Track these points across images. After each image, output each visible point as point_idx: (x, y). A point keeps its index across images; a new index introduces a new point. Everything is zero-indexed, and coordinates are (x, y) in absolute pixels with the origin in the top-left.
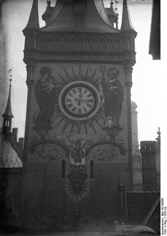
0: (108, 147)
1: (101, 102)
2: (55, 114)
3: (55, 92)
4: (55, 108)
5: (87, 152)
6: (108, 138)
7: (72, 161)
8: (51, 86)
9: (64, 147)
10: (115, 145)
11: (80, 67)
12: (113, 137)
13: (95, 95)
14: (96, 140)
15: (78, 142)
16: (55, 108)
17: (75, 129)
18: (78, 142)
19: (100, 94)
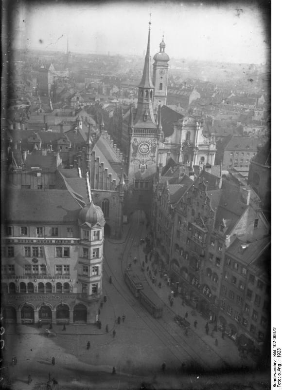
7: (141, 165)
8: (137, 144)
19: (150, 147)
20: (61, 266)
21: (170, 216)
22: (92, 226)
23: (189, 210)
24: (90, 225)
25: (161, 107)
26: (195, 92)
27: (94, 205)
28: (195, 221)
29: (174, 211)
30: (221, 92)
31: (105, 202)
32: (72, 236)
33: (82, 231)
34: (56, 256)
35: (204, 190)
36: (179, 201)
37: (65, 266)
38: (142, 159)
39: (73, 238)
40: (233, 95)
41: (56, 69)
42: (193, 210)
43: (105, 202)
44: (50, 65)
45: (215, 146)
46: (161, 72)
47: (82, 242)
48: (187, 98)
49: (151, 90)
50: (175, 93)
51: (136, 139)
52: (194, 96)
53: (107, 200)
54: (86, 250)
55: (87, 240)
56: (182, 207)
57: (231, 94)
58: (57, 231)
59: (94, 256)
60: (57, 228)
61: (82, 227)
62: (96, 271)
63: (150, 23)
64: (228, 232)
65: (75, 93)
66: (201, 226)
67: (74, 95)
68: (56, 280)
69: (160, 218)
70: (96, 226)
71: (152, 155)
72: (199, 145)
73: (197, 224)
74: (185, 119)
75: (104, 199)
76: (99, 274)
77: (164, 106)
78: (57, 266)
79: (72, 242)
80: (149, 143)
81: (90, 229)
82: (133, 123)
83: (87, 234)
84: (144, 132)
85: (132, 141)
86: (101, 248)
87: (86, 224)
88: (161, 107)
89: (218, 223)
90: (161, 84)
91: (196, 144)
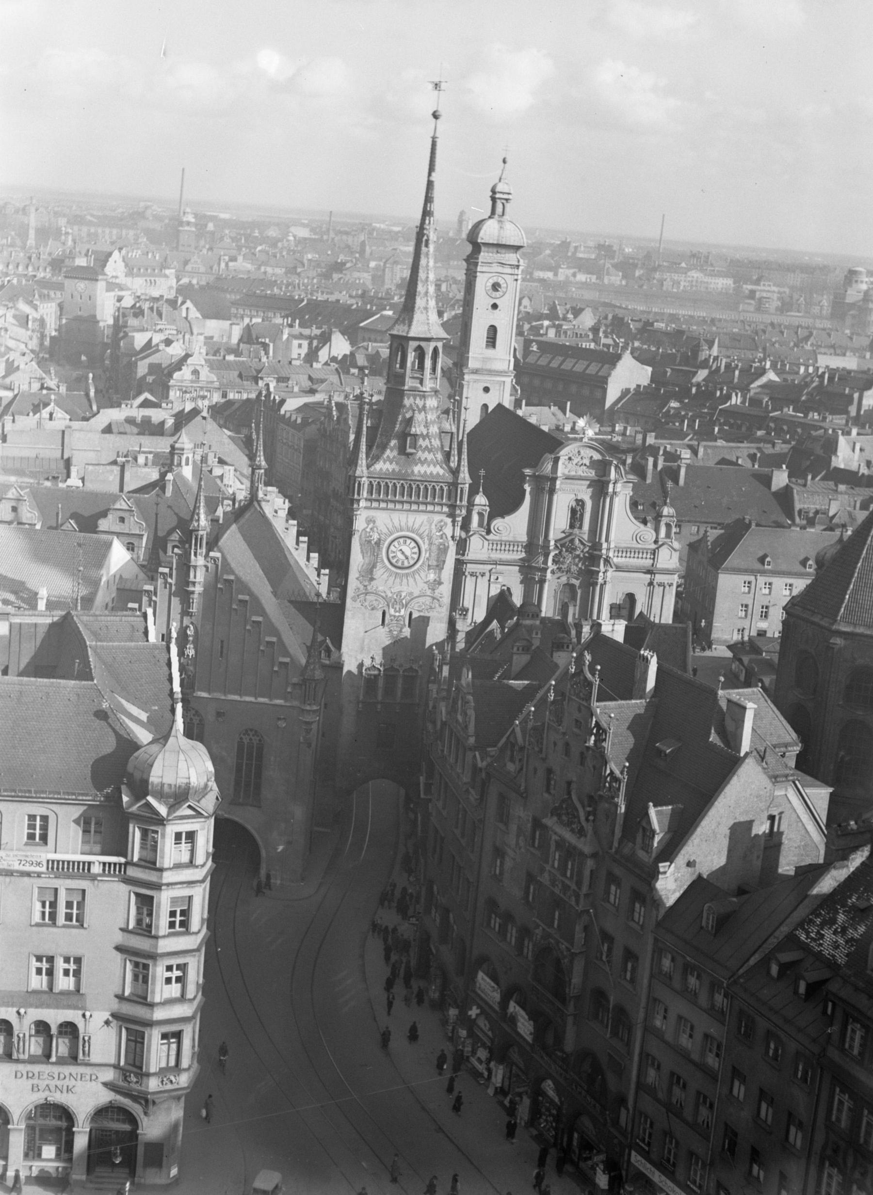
7: (392, 611)
8: (375, 537)
19: (424, 547)
20: (51, 959)
21: (474, 795)
22: (172, 808)
23: (535, 770)
24: (163, 810)
25: (490, 410)
26: (627, 362)
27: (612, 999)
28: (555, 812)
29: (483, 775)
30: (728, 366)
31: (246, 741)
32: (98, 848)
33: (136, 835)
34: (37, 918)
35: (588, 698)
36: (504, 740)
37: (67, 960)
38: (396, 589)
39: (103, 853)
40: (771, 376)
41: (130, 271)
42: (549, 771)
43: (246, 741)
44: (110, 254)
45: (676, 555)
46: (496, 287)
47: (132, 872)
48: (601, 383)
49: (432, 345)
50: (554, 364)
51: (371, 520)
52: (628, 375)
53: (256, 733)
54: (146, 903)
55: (150, 863)
56: (512, 760)
57: (762, 372)
58: (45, 828)
59: (172, 925)
60: (45, 819)
61: (138, 818)
62: (178, 979)
63: (436, 116)
64: (669, 852)
65: (187, 356)
66: (572, 831)
67: (179, 365)
68: (31, 1011)
69: (440, 804)
70: (185, 811)
71: (432, 576)
72: (618, 550)
73: (561, 822)
74: (564, 453)
75: (246, 732)
76: (190, 995)
77: (500, 406)
78: (39, 959)
79: (96, 869)
80: (420, 536)
81: (161, 821)
82: (363, 460)
83: (151, 845)
84: (406, 491)
85: (359, 524)
86: (200, 897)
87: (148, 805)
88: (490, 410)
89: (636, 822)
90: (493, 330)
91: (605, 545)
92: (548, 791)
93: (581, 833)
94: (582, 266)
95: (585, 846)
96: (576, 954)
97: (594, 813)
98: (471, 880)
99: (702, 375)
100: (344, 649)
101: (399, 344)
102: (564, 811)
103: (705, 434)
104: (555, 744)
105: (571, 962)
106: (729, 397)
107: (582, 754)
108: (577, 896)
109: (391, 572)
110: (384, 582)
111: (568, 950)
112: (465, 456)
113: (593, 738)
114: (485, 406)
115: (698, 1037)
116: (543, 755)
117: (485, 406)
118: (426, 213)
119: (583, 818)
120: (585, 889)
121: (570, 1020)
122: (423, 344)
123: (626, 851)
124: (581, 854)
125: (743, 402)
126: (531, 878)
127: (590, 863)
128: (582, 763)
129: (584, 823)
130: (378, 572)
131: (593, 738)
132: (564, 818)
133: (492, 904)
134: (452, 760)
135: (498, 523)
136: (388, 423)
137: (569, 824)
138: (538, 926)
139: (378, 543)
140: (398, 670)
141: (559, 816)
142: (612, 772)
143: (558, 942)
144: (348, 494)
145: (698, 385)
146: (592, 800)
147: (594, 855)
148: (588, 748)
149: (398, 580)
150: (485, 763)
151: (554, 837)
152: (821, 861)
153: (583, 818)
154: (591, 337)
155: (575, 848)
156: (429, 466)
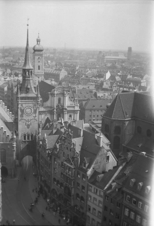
0: (34, 120)
1: (33, 111)
2: (24, 114)
3: (24, 109)
4: (48, 151)
5: (30, 121)
6: (34, 118)
7: (27, 123)
8: (23, 108)
9: (26, 120)
10: (35, 119)
11: (101, 123)
12: (35, 118)
13: (31, 110)
14: (32, 119)
15: (28, 119)
16: (48, 151)
17: (28, 117)
18: (28, 119)
19: (32, 109)
21: (49, 158)
23: (61, 153)
25: (40, 82)
26: (63, 70)
28: (66, 161)
30: (81, 70)
63: (28, 25)
64: (89, 167)
66: (70, 164)
69: (42, 160)
71: (34, 115)
73: (67, 163)
88: (40, 82)
91: (65, 106)
92: (64, 157)
93: (71, 164)
94: (51, 53)
95: (72, 167)
96: (72, 188)
97: (74, 160)
98: (50, 175)
99: (76, 73)
100: (19, 131)
101: (24, 71)
102: (68, 161)
103: (79, 84)
104: (65, 147)
105: (72, 189)
106: (82, 76)
107: (70, 149)
108: (72, 176)
109: (27, 115)
110: (25, 117)
111: (71, 187)
112: (39, 91)
113: (72, 146)
114: (39, 81)
115: (98, 201)
116: (62, 150)
117: (39, 81)
118: (27, 44)
119: (72, 161)
120: (73, 175)
121: (72, 200)
122: (29, 70)
123: (81, 167)
124: (72, 168)
125: (85, 77)
126: (62, 174)
127: (74, 170)
128: (71, 151)
129: (72, 162)
130: (24, 115)
131: (72, 146)
132: (68, 162)
133: (55, 179)
134: (43, 152)
135: (44, 103)
136: (23, 87)
137: (69, 163)
138: (64, 183)
139: (24, 109)
140: (29, 134)
141: (67, 161)
142: (77, 152)
143: (68, 185)
144: (17, 100)
145: (76, 74)
146: (73, 158)
147: (74, 168)
148: (72, 148)
149: (28, 117)
150: (51, 152)
151: (66, 166)
152: (116, 165)
153: (72, 161)
154: (55, 67)
155: (71, 167)
156: (33, 94)
